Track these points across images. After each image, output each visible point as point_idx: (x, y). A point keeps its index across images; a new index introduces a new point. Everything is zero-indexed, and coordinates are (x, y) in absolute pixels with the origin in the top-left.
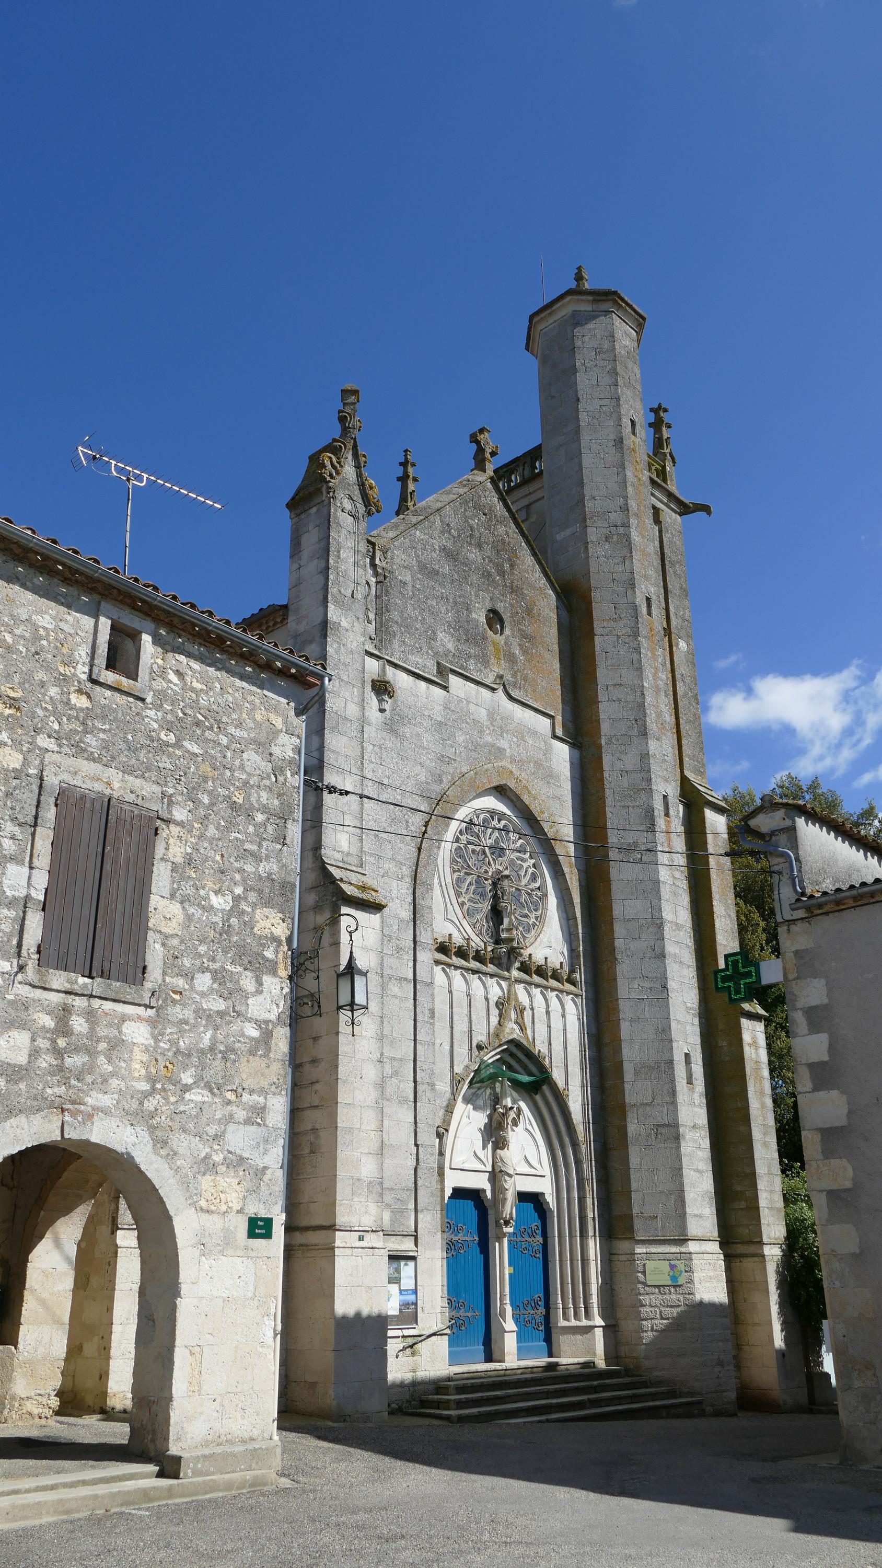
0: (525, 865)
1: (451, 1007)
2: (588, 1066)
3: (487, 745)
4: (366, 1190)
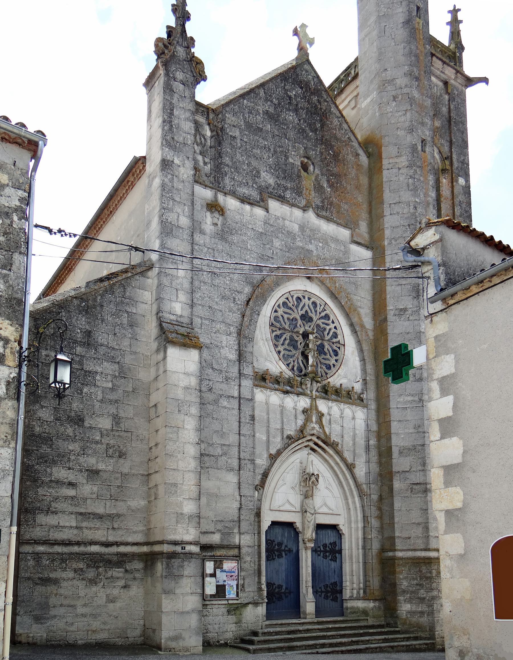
0: (328, 328)
3: (298, 247)
4: (187, 520)
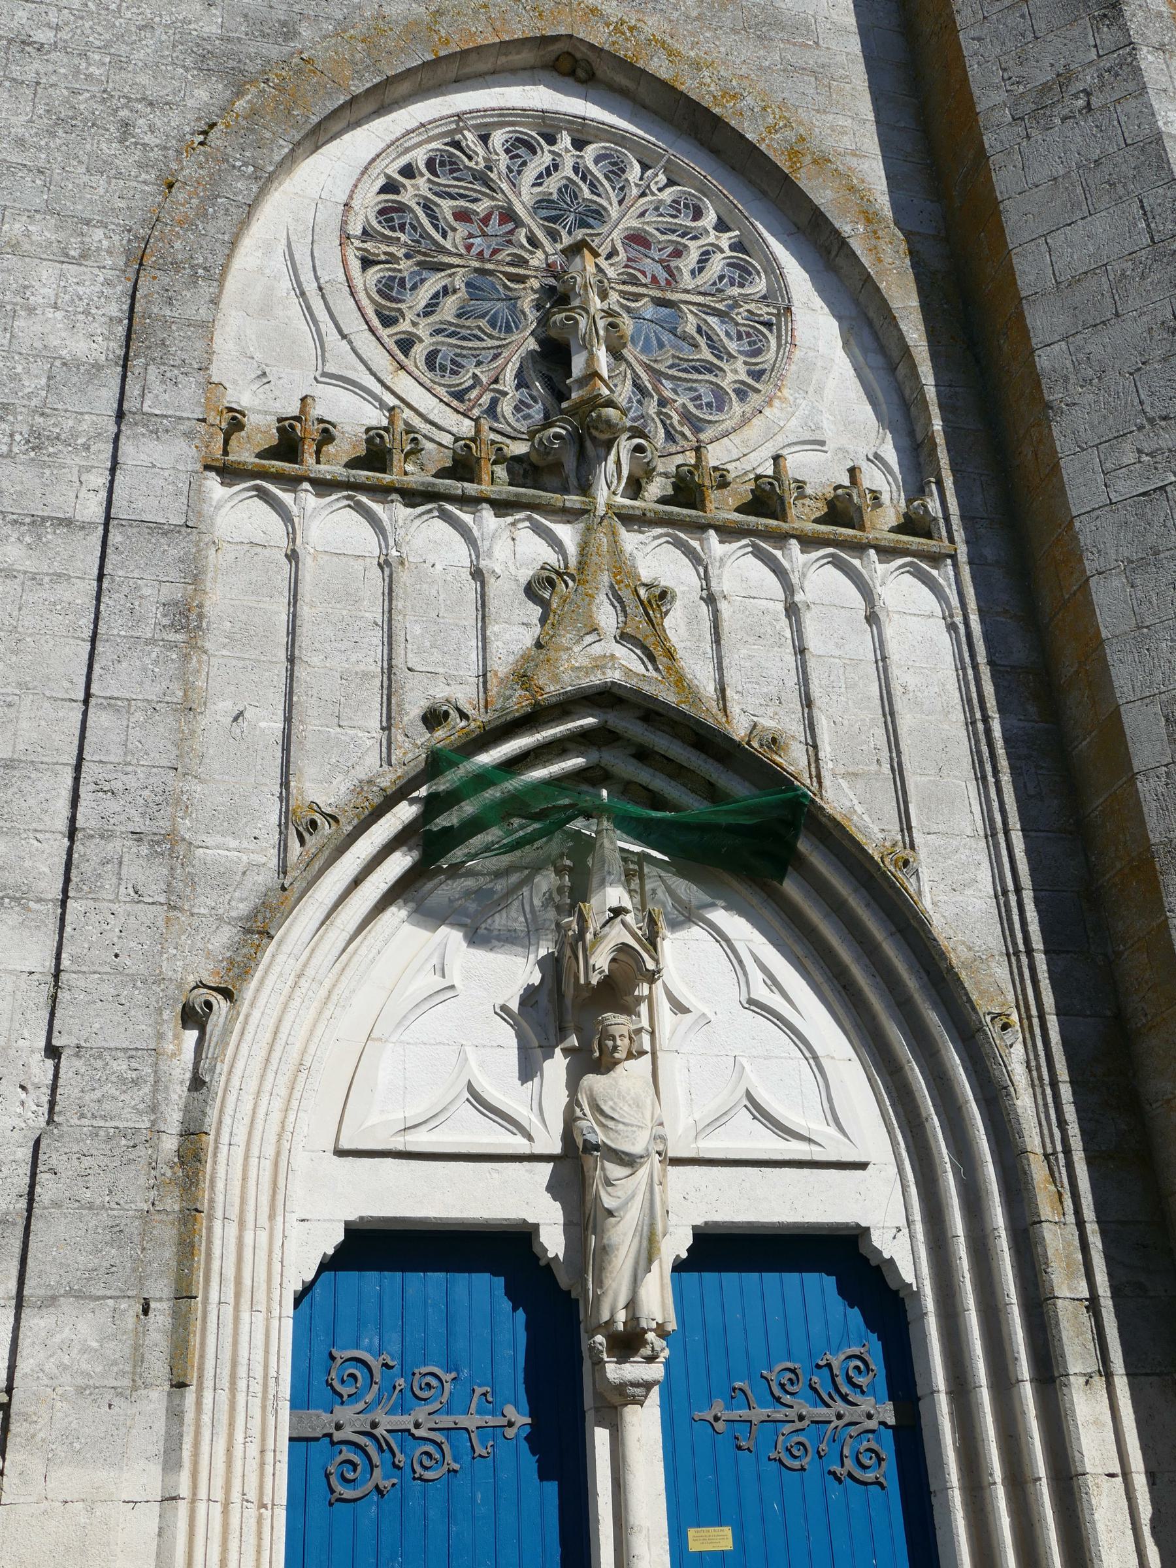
1: (294, 600)
2: (1003, 763)
